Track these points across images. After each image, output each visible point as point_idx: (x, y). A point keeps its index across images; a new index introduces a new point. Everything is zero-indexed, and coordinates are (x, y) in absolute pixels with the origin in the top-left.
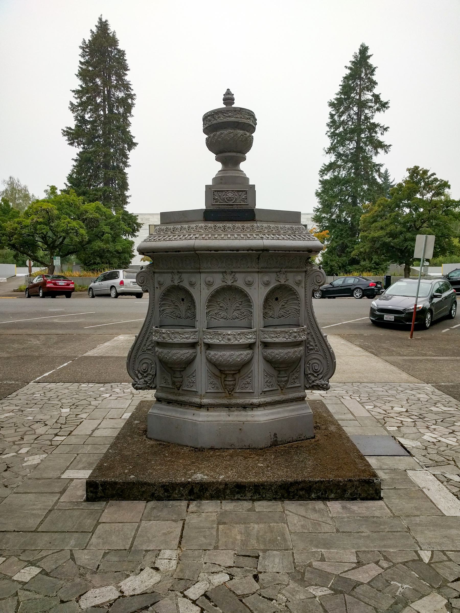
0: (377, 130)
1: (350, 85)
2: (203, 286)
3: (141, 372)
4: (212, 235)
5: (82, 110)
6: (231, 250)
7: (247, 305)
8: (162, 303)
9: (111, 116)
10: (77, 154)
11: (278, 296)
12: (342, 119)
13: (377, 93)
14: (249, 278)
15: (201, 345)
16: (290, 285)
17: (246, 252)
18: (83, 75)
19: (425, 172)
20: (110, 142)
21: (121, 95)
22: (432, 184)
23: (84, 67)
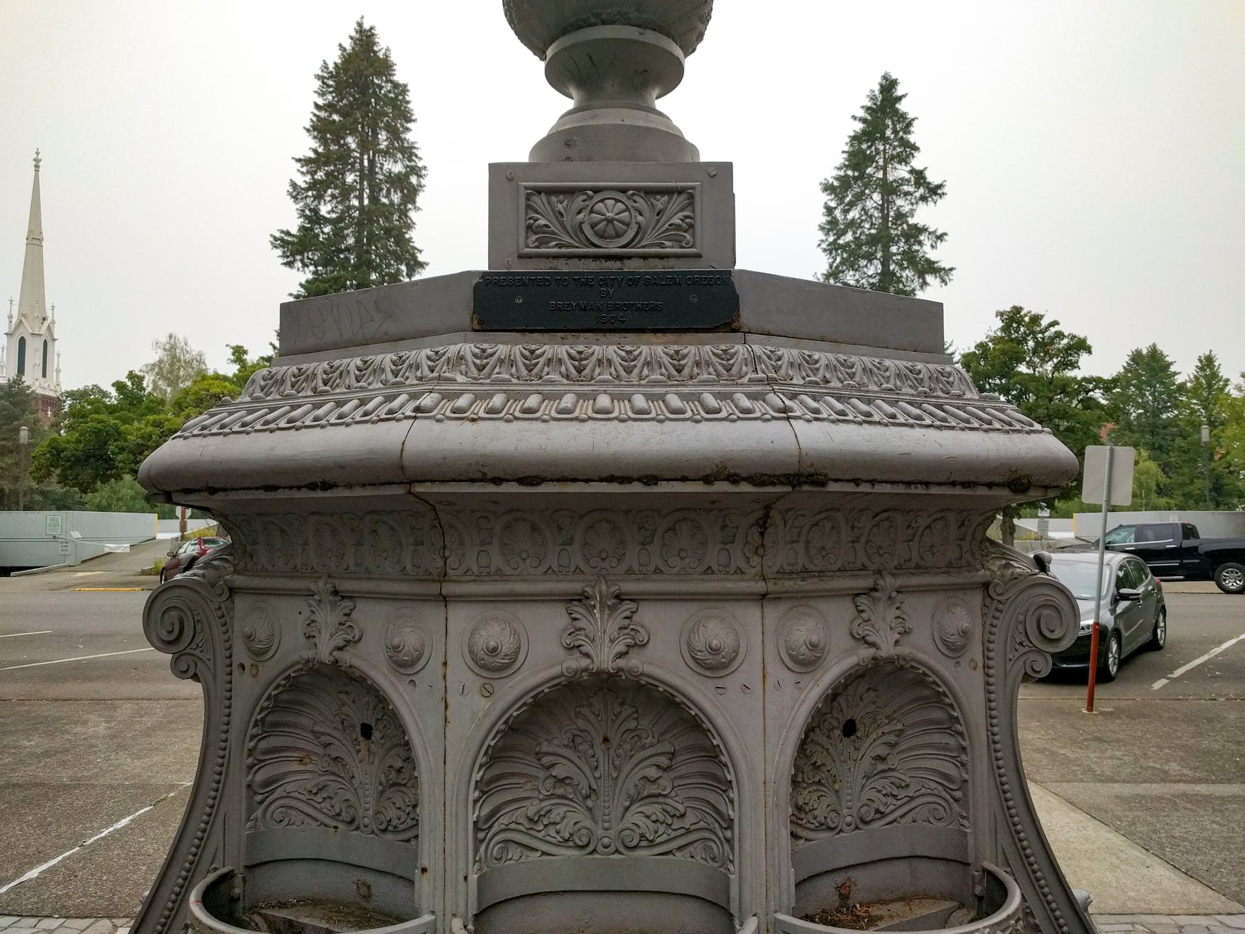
0: (922, 238)
1: (863, 152)
2: (461, 673)
4: (513, 396)
5: (315, 197)
6: (610, 479)
7: (702, 774)
8: (263, 745)
9: (374, 207)
10: (301, 285)
11: (856, 714)
12: (850, 216)
13: (918, 167)
14: (715, 631)
16: (921, 656)
17: (699, 487)
18: (320, 128)
19: (1036, 319)
20: (370, 262)
21: (398, 168)
22: (1052, 343)
23: (323, 114)
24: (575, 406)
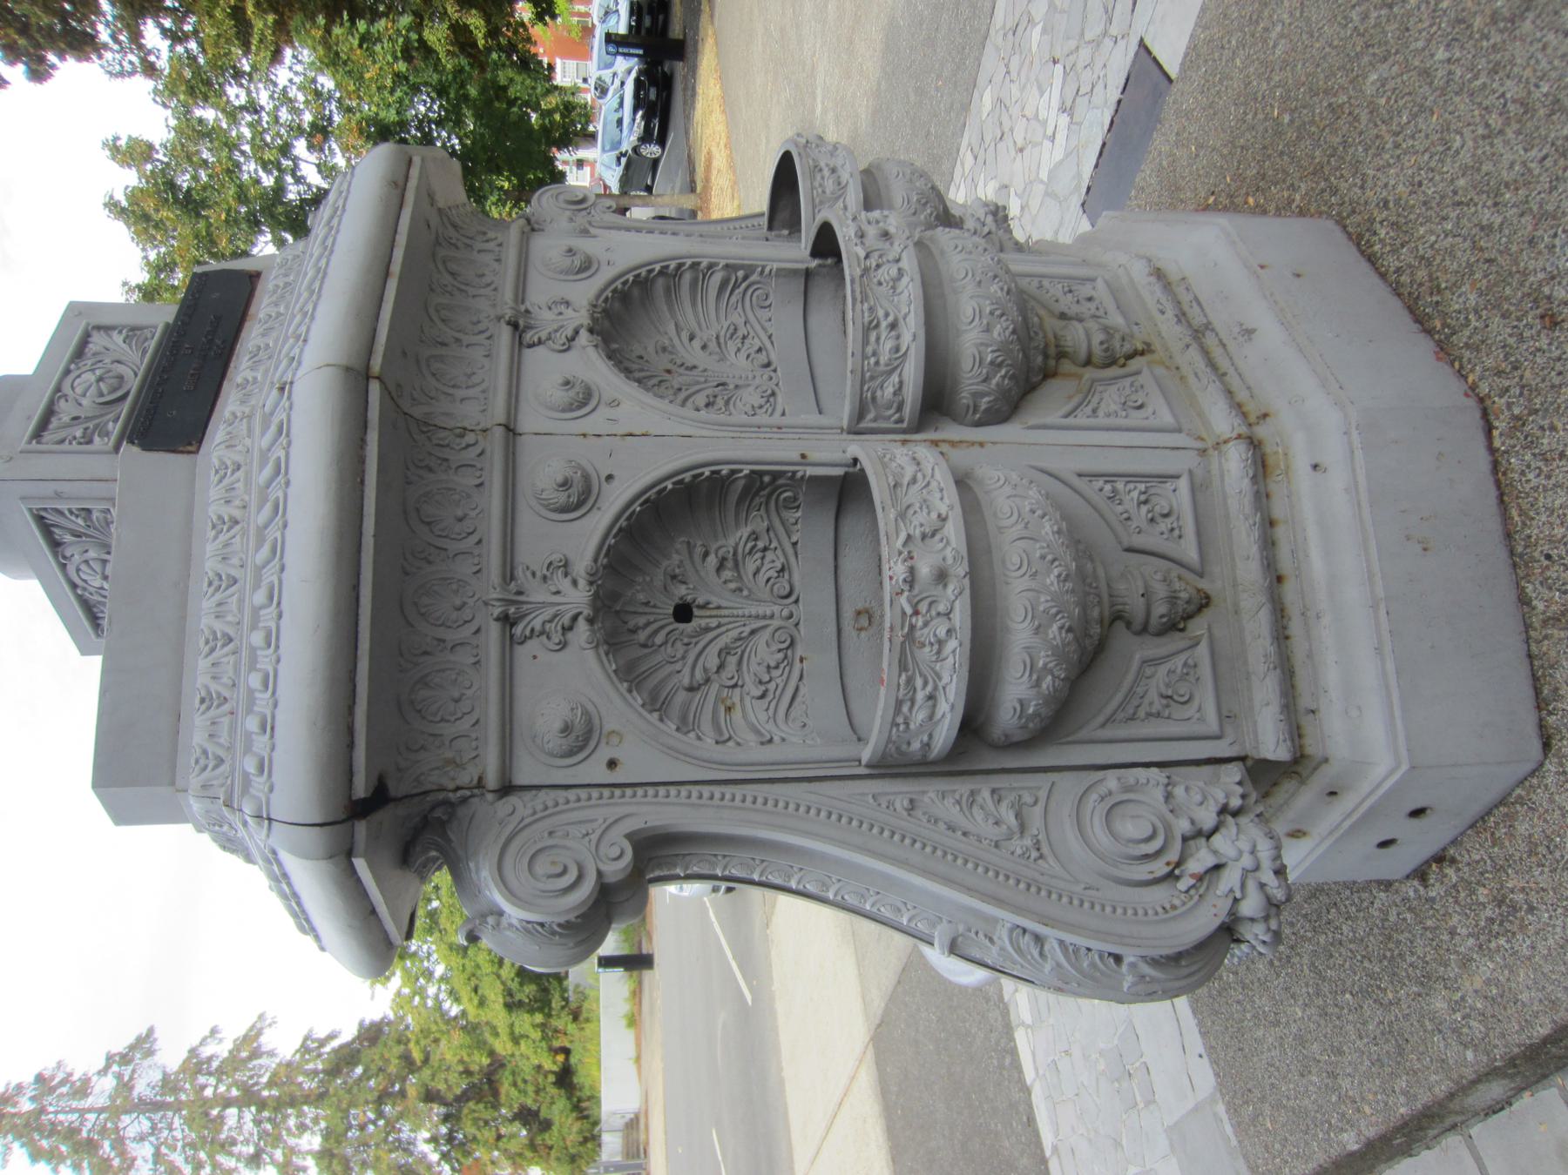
2: (596, 422)
3: (1173, 855)
7: (694, 304)
24: (255, 797)
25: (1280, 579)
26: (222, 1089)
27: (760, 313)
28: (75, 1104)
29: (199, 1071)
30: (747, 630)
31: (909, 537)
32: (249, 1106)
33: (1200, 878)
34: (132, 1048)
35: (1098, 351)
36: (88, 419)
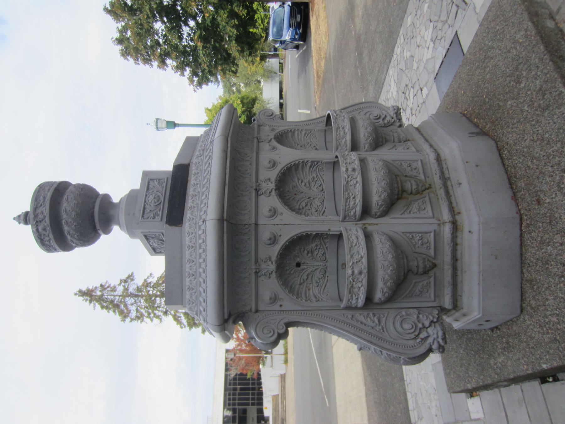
2: (277, 220)
3: (417, 333)
15: (364, 224)
25: (457, 260)
26: (155, 292)
27: (321, 173)
28: (112, 293)
29: (147, 286)
30: (314, 269)
31: (353, 263)
32: (163, 297)
33: (422, 339)
34: (127, 278)
35: (414, 191)
36: (154, 210)
